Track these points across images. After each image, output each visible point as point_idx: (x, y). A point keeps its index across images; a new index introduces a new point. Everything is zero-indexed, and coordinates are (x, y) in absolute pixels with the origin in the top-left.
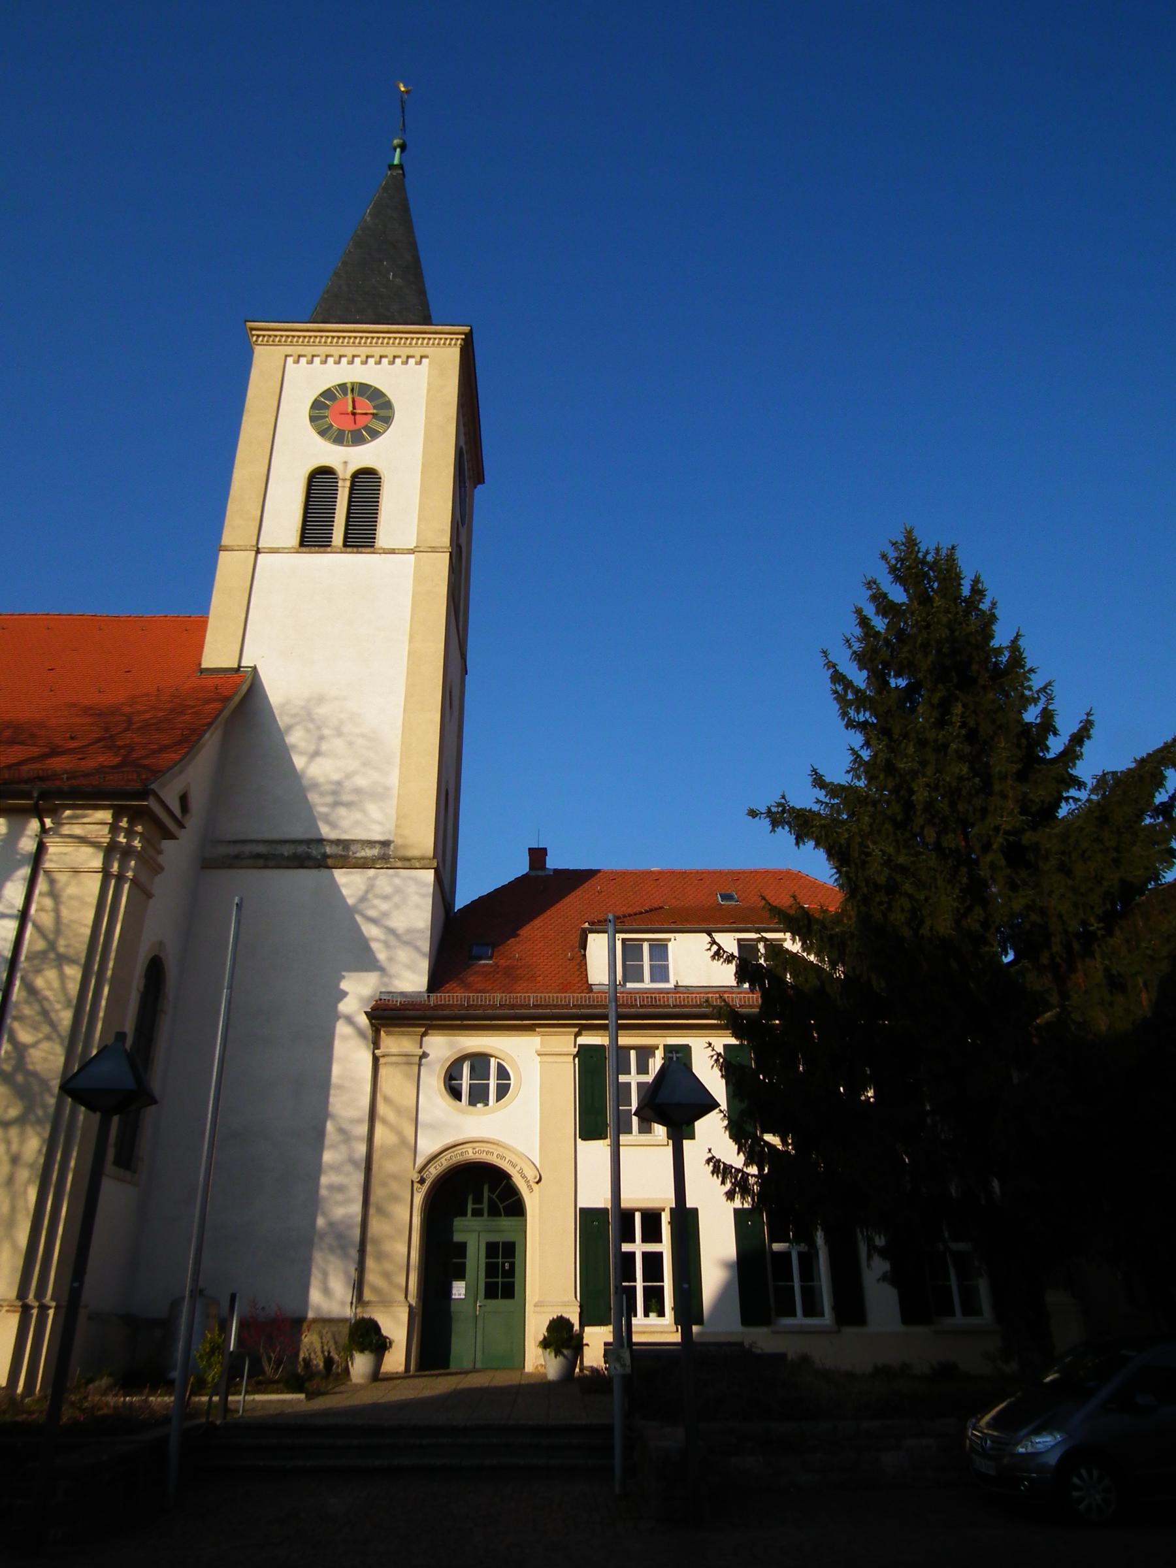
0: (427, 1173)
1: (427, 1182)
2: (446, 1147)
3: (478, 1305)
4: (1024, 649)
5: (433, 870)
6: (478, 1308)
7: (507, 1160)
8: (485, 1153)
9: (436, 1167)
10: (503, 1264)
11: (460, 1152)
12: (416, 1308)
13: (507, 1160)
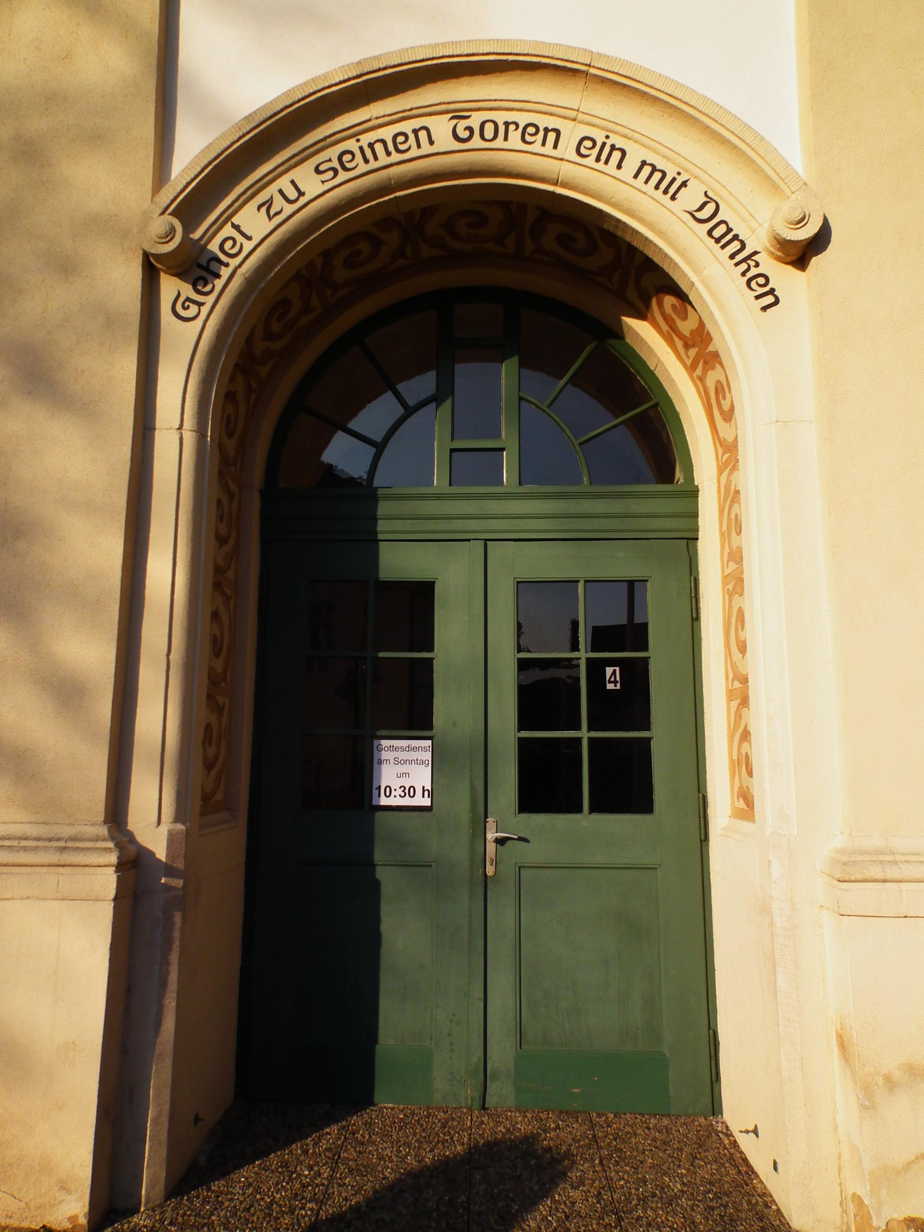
0: (227, 231)
1: (225, 273)
2: (482, 1097)
3: (491, 836)
4: (423, 797)
5: (430, 805)
6: (491, 848)
7: (631, 164)
8: (515, 136)
9: (269, 203)
10: (596, 668)
11: (387, 133)
12: (168, 869)
13: (631, 164)
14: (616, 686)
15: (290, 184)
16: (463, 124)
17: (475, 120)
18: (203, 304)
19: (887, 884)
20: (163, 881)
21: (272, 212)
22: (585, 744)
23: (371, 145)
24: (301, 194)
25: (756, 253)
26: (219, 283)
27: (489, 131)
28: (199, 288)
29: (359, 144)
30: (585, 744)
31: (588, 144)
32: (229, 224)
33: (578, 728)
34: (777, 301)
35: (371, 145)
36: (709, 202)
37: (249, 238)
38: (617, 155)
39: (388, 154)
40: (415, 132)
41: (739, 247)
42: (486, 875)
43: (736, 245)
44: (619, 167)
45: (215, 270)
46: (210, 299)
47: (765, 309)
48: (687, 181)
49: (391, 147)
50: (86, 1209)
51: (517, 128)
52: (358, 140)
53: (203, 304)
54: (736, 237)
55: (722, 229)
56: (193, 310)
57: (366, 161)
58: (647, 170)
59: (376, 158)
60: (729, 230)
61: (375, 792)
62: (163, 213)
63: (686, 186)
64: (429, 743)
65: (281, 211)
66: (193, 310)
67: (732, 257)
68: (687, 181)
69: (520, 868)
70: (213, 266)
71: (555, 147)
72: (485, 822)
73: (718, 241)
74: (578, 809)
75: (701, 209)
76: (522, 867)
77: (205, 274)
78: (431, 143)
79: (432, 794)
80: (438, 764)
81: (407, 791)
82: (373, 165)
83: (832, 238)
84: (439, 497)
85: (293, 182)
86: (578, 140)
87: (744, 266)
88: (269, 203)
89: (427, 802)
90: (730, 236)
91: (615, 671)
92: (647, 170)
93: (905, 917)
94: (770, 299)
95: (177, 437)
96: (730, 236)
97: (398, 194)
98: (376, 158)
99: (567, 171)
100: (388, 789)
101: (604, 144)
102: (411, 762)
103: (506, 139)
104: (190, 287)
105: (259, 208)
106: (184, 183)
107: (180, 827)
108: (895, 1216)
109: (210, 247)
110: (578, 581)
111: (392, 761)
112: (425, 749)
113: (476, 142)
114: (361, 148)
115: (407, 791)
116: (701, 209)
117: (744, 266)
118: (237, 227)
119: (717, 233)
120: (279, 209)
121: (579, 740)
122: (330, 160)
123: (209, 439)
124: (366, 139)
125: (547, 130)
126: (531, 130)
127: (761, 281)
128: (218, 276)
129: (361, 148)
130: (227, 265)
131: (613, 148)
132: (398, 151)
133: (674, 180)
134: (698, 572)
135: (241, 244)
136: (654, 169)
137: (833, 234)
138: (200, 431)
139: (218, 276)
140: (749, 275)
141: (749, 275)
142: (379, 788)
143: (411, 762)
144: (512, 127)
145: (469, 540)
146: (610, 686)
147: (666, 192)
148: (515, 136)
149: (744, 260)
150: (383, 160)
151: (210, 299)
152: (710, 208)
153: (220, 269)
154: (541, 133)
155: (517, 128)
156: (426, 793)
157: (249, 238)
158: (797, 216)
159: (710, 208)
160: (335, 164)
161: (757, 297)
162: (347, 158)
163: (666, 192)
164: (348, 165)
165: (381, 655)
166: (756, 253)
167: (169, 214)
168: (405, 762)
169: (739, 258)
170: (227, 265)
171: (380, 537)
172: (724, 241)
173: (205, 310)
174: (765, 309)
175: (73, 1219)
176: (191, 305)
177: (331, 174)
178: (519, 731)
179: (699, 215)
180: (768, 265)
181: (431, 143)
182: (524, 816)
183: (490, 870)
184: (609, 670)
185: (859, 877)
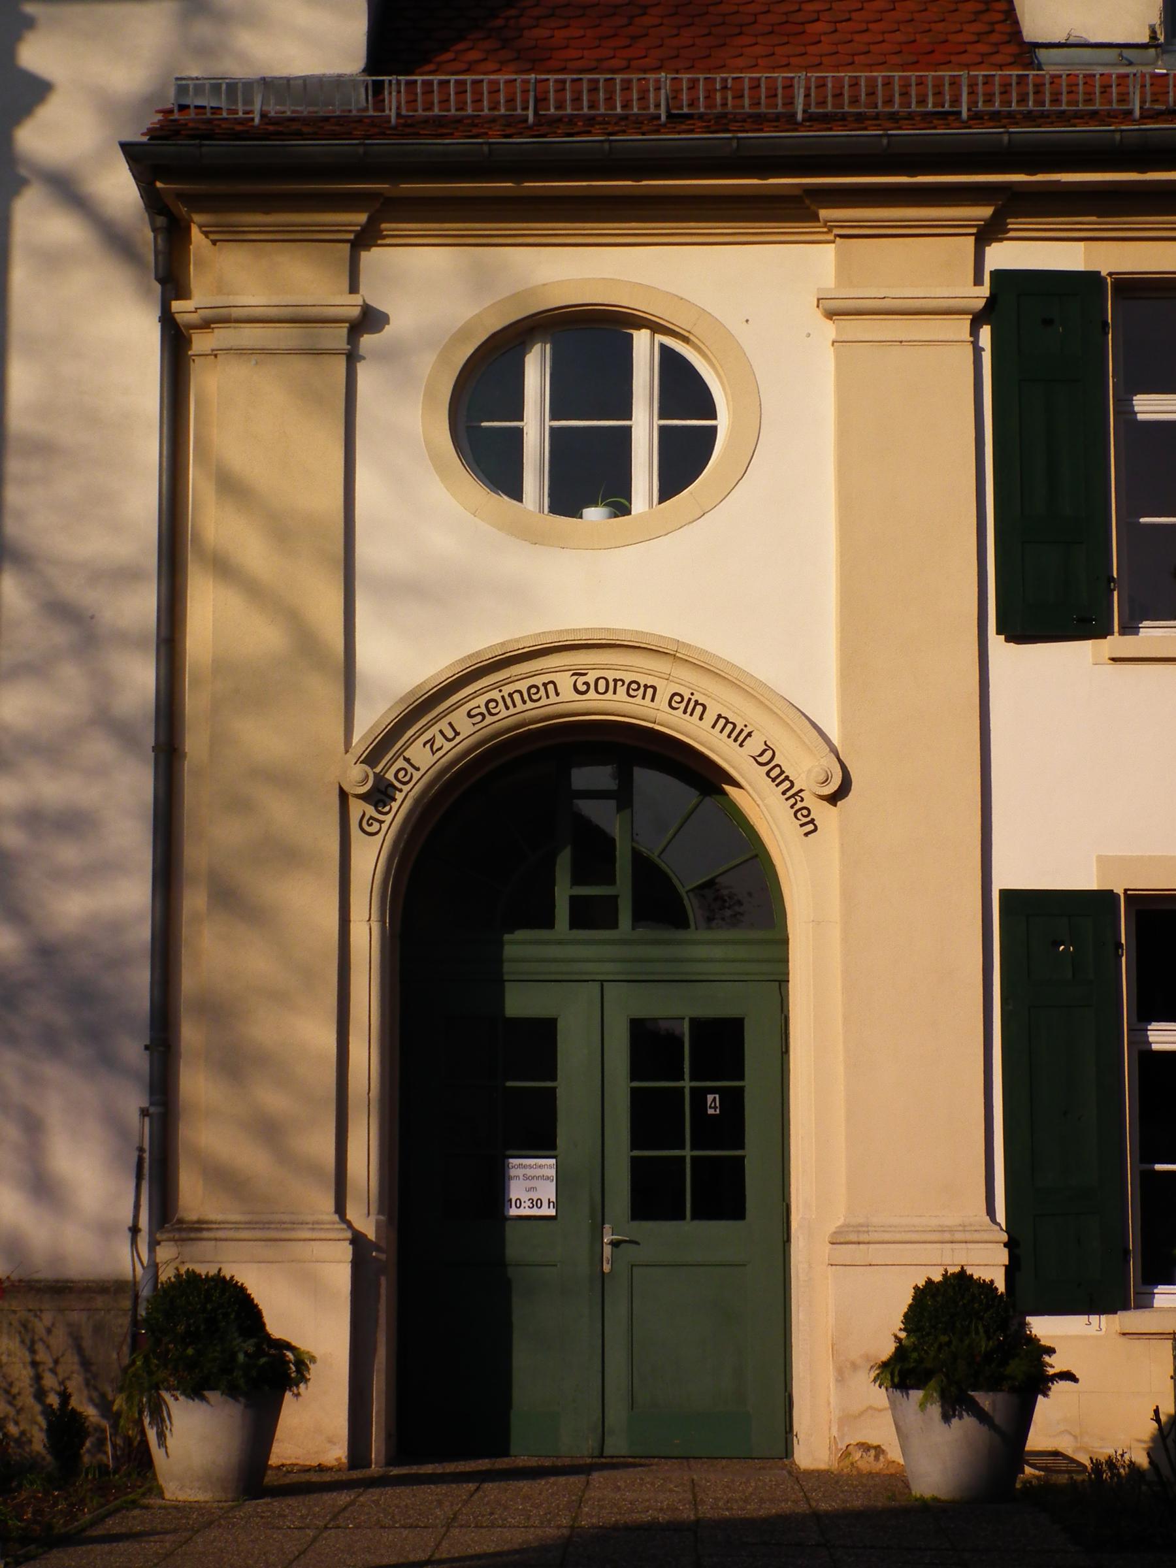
0: (401, 763)
1: (399, 796)
4: (549, 1207)
6: (607, 1250)
7: (710, 717)
9: (432, 741)
10: (699, 1096)
13: (710, 717)
14: (715, 1111)
15: (448, 726)
16: (582, 679)
17: (591, 678)
18: (384, 822)
19: (861, 1246)
20: (374, 1254)
21: (435, 748)
22: (688, 1160)
23: (510, 695)
24: (457, 734)
25: (801, 791)
26: (395, 805)
27: (602, 686)
28: (380, 809)
29: (501, 694)
30: (688, 1160)
31: (678, 698)
32: (402, 757)
33: (683, 1147)
34: (816, 829)
35: (510, 695)
36: (767, 750)
37: (418, 769)
38: (699, 709)
39: (524, 702)
40: (545, 685)
41: (789, 785)
42: (603, 1272)
43: (787, 784)
44: (701, 718)
45: (392, 794)
46: (389, 818)
47: (806, 834)
48: (751, 732)
49: (526, 697)
50: (346, 1454)
51: (623, 685)
52: (500, 691)
53: (384, 822)
54: (787, 778)
55: (777, 771)
56: (376, 826)
57: (507, 708)
58: (722, 722)
59: (515, 706)
60: (782, 772)
61: (507, 1204)
62: (355, 763)
63: (751, 736)
64: (553, 1161)
65: (442, 747)
66: (376, 826)
67: (784, 793)
68: (751, 732)
69: (632, 1266)
70: (390, 790)
71: (653, 700)
72: (603, 1228)
73: (774, 780)
74: (682, 1217)
75: (761, 755)
76: (635, 1265)
77: (383, 797)
78: (557, 694)
79: (557, 1206)
80: (562, 1181)
81: (535, 1203)
82: (512, 711)
83: (853, 788)
84: (560, 942)
85: (450, 724)
86: (670, 695)
87: (792, 801)
88: (432, 741)
89: (552, 1212)
90: (782, 777)
91: (715, 1098)
92: (722, 722)
93: (870, 1265)
94: (811, 827)
95: (368, 928)
96: (782, 777)
97: (531, 727)
98: (515, 706)
99: (660, 716)
100: (518, 1201)
101: (690, 700)
102: (538, 1178)
103: (615, 693)
104: (373, 808)
105: (424, 745)
106: (374, 737)
107: (382, 1217)
108: (852, 1442)
109: (386, 776)
110: (684, 1019)
111: (521, 1177)
112: (550, 1167)
113: (592, 694)
114: (503, 697)
115: (535, 1203)
116: (761, 755)
117: (792, 801)
118: (407, 760)
119: (773, 774)
120: (440, 746)
121: (684, 1158)
122: (479, 707)
123: (388, 925)
124: (507, 690)
125: (646, 687)
126: (634, 686)
127: (805, 812)
128: (395, 800)
129: (503, 697)
130: (401, 791)
131: (697, 703)
132: (532, 700)
133: (742, 730)
134: (789, 1011)
135: (412, 774)
136: (727, 722)
137: (853, 784)
138: (382, 921)
139: (395, 800)
140: (796, 807)
141: (796, 807)
142: (511, 1200)
143: (538, 1178)
144: (619, 683)
145: (588, 981)
146: (711, 1111)
147: (735, 740)
148: (622, 690)
149: (793, 796)
150: (520, 707)
151: (389, 818)
152: (769, 754)
153: (395, 794)
154: (642, 689)
155: (623, 685)
156: (552, 1204)
157: (418, 769)
158: (822, 778)
159: (769, 754)
160: (483, 710)
161: (802, 825)
162: (492, 705)
163: (735, 740)
164: (493, 711)
165: (509, 1084)
166: (801, 791)
167: (361, 763)
168: (533, 1178)
169: (789, 794)
170: (401, 791)
171: (506, 977)
172: (778, 781)
173: (385, 827)
174: (806, 834)
175: (338, 1459)
176: (374, 822)
177: (480, 718)
178: (631, 1151)
179: (760, 759)
180: (809, 801)
181: (557, 694)
182: (636, 1224)
183: (607, 1268)
184: (710, 1097)
185: (842, 1240)
